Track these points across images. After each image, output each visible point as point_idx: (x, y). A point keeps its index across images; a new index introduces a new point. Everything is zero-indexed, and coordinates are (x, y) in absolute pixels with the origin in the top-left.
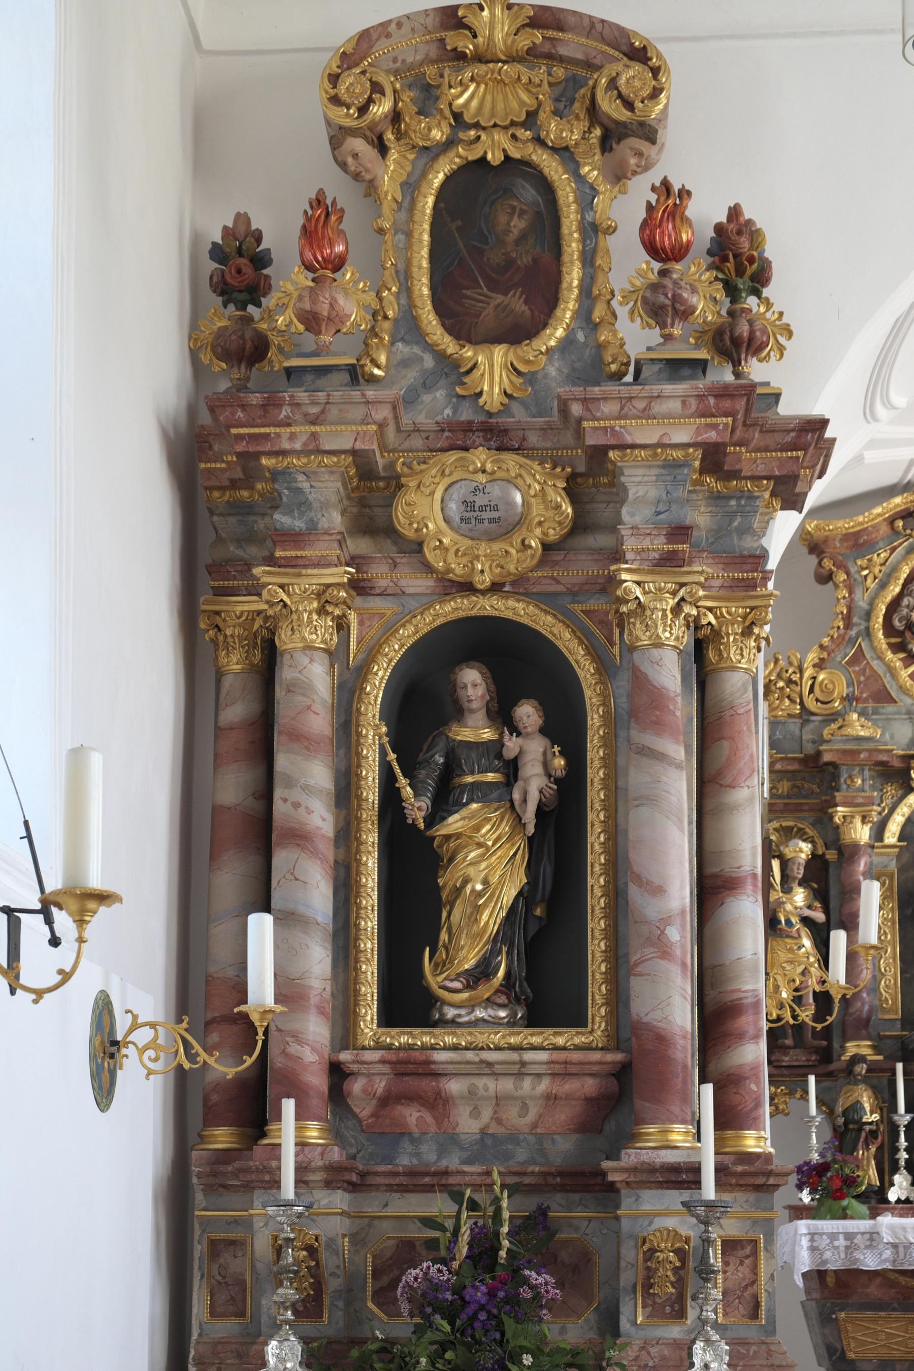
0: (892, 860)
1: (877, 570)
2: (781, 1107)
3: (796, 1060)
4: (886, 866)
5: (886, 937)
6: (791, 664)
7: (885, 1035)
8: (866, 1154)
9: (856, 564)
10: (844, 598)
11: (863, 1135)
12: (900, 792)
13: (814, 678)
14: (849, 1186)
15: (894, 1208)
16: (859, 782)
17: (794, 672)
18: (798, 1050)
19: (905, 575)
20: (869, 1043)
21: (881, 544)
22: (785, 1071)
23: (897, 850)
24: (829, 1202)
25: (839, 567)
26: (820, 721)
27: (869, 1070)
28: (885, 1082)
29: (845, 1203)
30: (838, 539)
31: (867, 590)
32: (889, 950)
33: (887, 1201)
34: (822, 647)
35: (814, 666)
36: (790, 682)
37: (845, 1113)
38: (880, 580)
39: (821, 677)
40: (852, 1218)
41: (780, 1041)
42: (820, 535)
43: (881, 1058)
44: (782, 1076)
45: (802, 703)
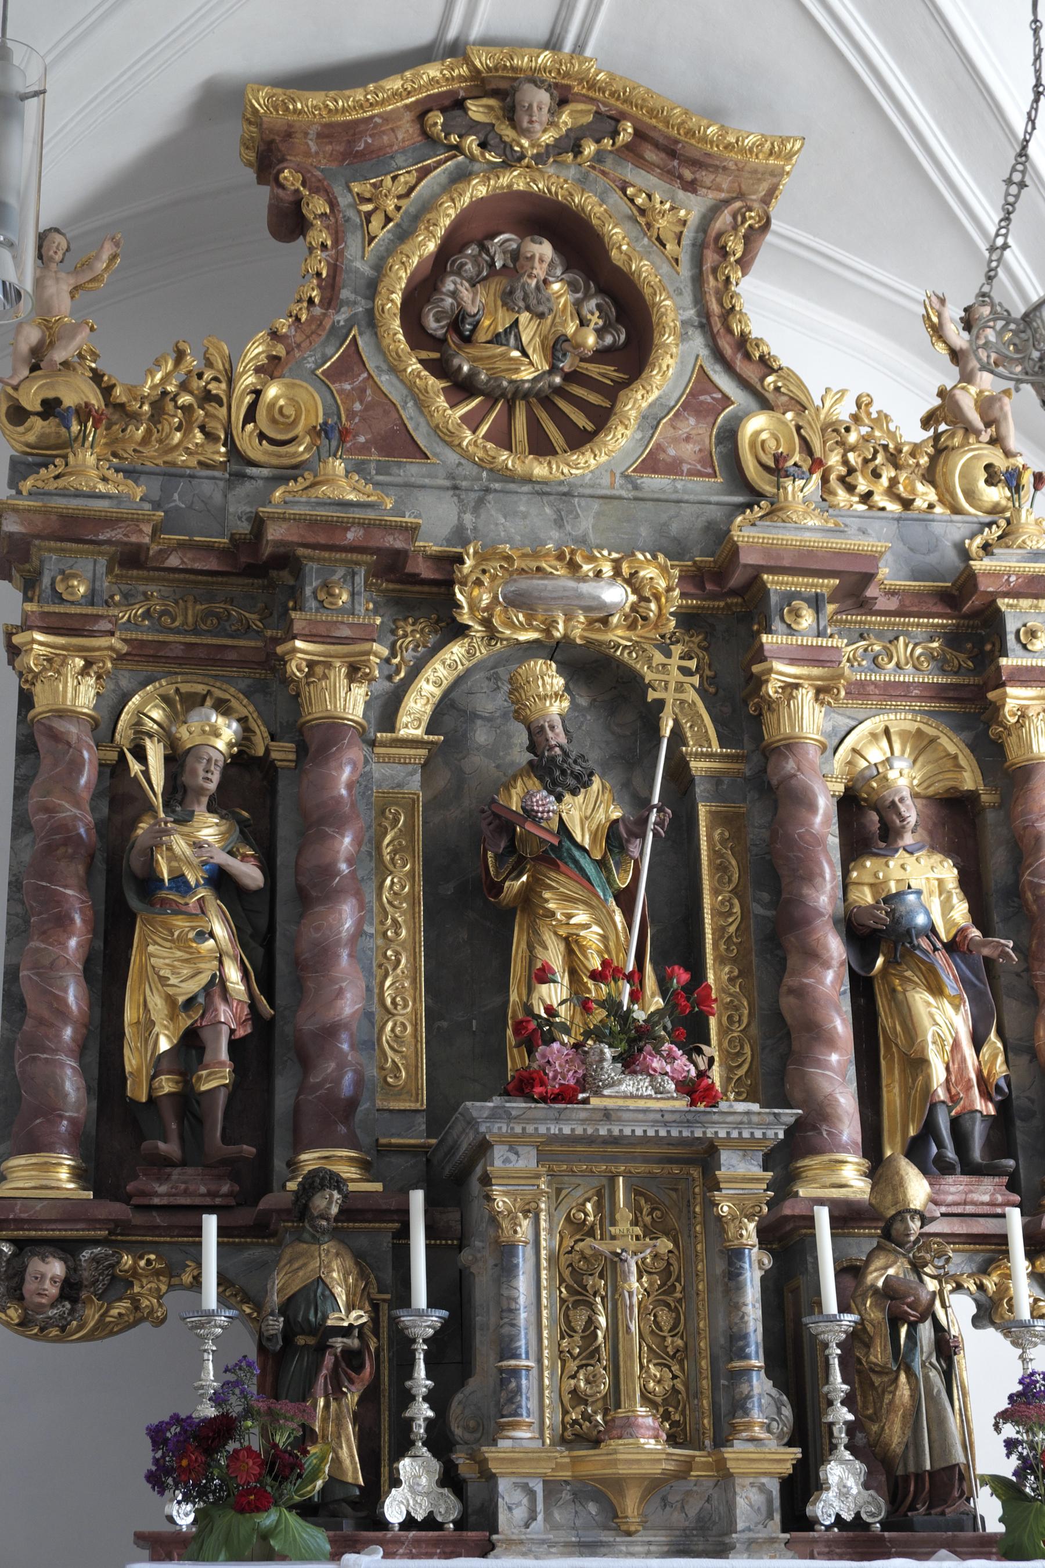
0: (412, 774)
1: (390, 205)
2: (145, 1303)
3: (186, 1193)
4: (399, 786)
5: (397, 934)
6: (209, 364)
7: (390, 1145)
8: (333, 1406)
9: (350, 191)
10: (324, 246)
11: (329, 1360)
12: (432, 639)
13: (258, 393)
14: (281, 1478)
15: (397, 1541)
16: (345, 597)
17: (216, 379)
18: (190, 1170)
19: (448, 222)
20: (353, 1154)
21: (400, 160)
22: (158, 1219)
23: (424, 752)
24: (227, 1518)
25: (315, 190)
26: (267, 479)
27: (345, 1213)
28: (386, 1242)
29: (268, 1519)
30: (312, 132)
31: (372, 239)
32: (403, 961)
33: (383, 1524)
34: (274, 335)
35: (258, 370)
36: (207, 397)
37: (286, 1308)
38: (397, 225)
39: (272, 391)
40: (283, 1558)
41: (146, 1145)
42: (277, 119)
43: (378, 1187)
44: (153, 1229)
45: (230, 442)
